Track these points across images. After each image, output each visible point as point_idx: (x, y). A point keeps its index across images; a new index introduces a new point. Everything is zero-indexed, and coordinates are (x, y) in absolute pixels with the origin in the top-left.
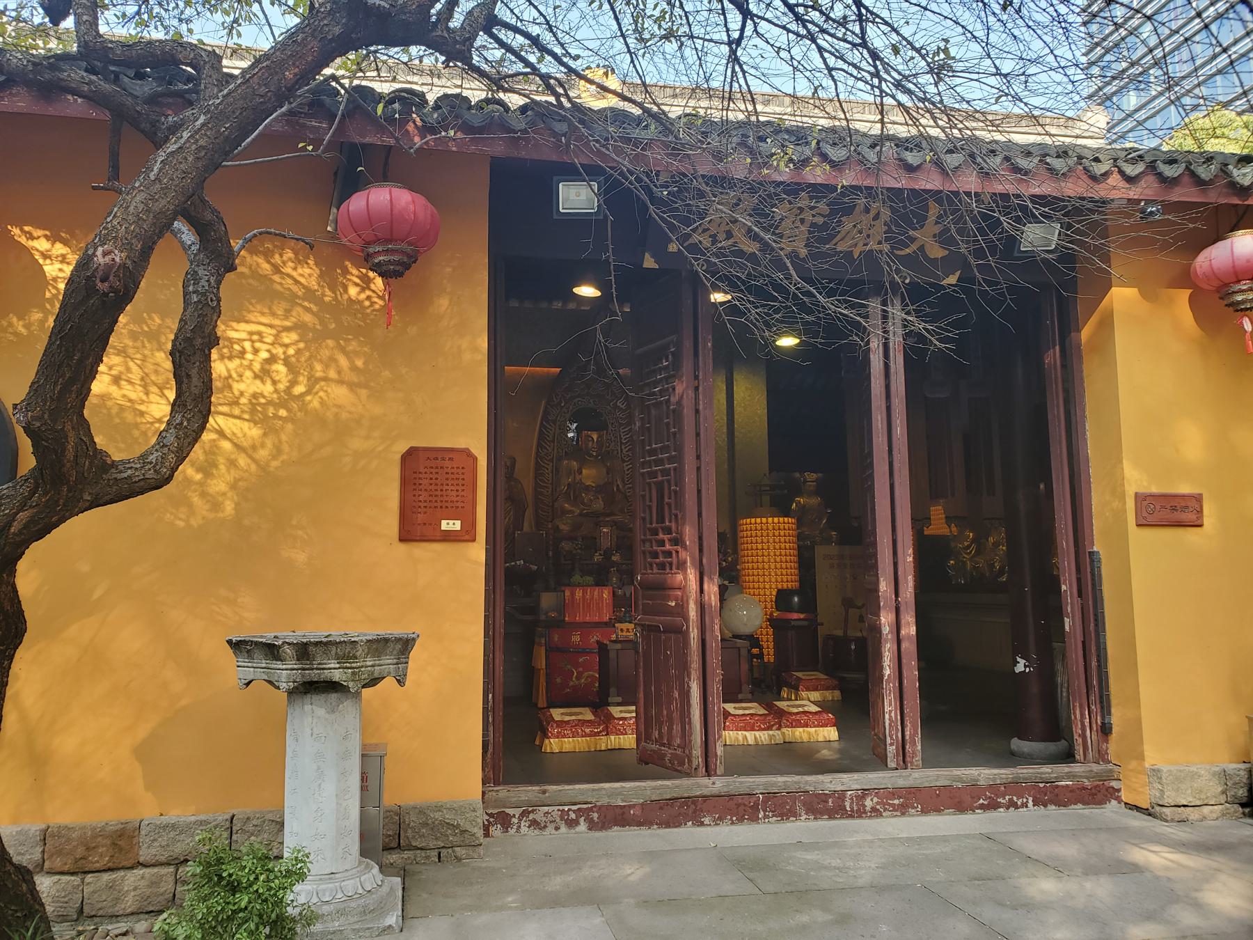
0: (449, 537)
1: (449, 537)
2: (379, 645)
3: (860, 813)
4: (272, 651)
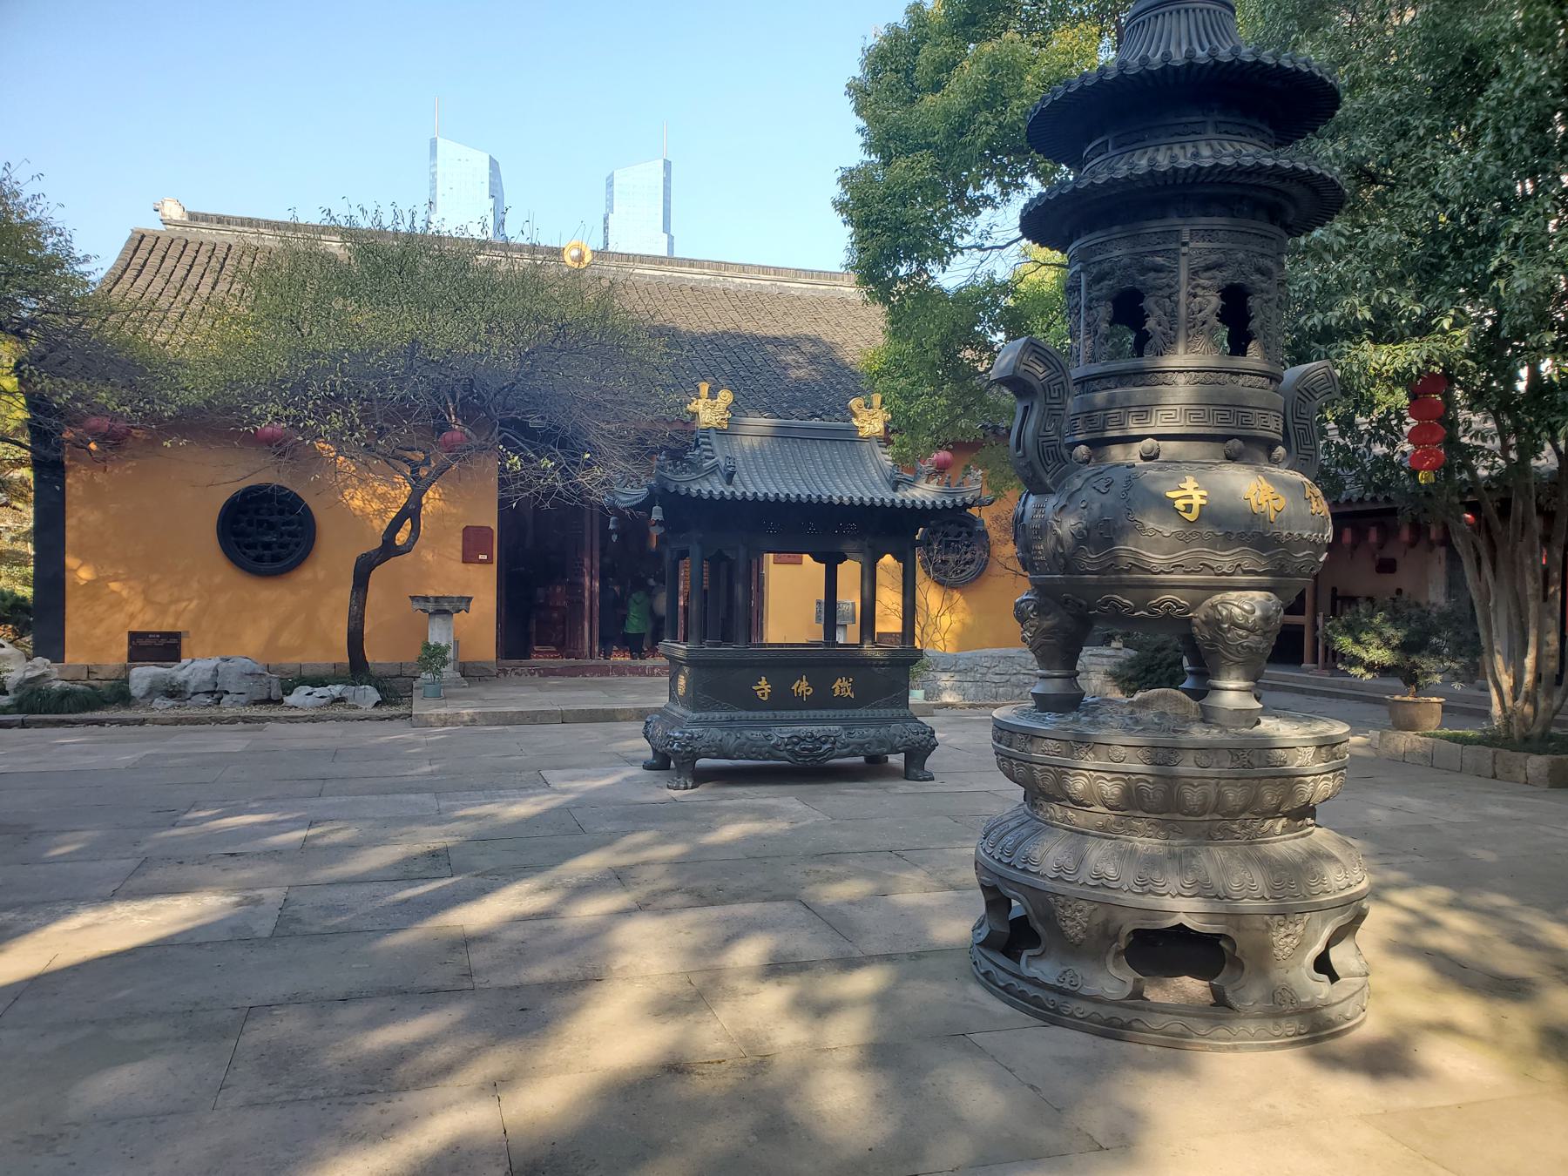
0: (482, 562)
1: (482, 562)
2: (461, 599)
3: (652, 675)
4: (426, 599)
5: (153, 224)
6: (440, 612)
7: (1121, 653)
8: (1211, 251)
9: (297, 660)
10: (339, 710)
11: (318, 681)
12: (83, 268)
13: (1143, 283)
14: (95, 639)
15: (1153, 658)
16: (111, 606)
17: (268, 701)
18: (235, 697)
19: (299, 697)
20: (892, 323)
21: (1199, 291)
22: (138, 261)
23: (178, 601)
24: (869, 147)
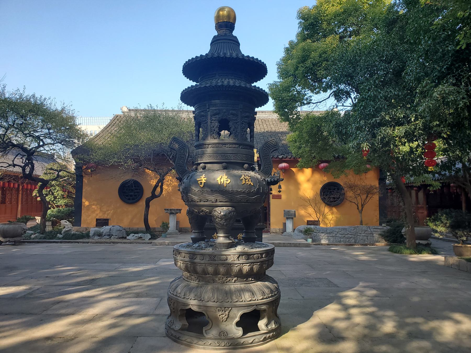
2: (177, 210)
4: (168, 210)
5: (120, 113)
6: (171, 213)
7: (385, 228)
8: (215, 110)
9: (137, 227)
10: (140, 241)
11: (136, 232)
12: (79, 126)
13: (229, 118)
14: (88, 219)
15: (395, 230)
16: (92, 212)
17: (123, 238)
18: (115, 236)
19: (131, 237)
20: (290, 127)
21: (213, 122)
22: (112, 124)
23: (108, 210)
24: (279, 77)
